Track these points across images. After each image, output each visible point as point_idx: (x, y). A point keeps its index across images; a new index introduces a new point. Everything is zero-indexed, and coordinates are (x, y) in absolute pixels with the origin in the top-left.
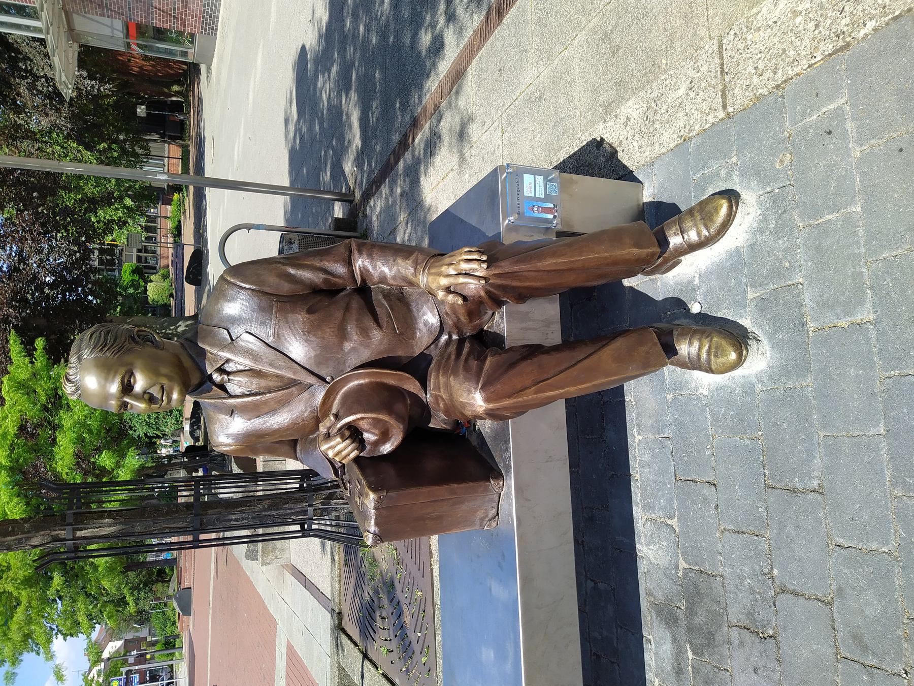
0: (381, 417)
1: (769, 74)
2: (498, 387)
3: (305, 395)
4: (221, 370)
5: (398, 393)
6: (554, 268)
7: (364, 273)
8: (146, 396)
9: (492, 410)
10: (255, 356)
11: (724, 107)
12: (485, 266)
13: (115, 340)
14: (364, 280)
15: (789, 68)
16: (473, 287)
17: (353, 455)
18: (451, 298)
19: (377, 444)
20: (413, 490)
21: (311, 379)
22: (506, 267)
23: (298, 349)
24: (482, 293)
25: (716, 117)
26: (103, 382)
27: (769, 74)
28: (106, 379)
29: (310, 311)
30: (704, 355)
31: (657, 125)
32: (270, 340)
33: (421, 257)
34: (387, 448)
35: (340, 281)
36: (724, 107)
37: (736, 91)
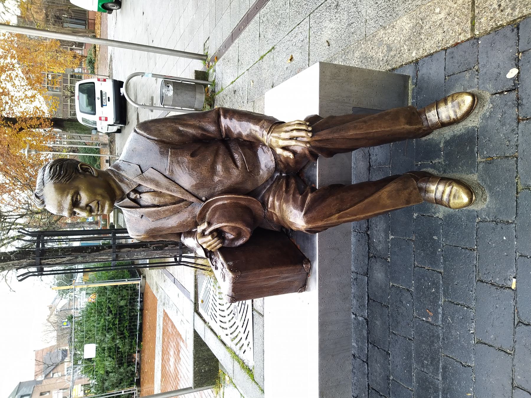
0: (237, 225)
1: (509, 11)
2: (314, 214)
3: (190, 208)
4: (135, 191)
5: (247, 209)
6: (355, 137)
7: (228, 130)
8: (88, 208)
9: (310, 228)
10: (157, 184)
11: (473, 30)
12: (310, 135)
13: (66, 172)
14: (227, 135)
15: (524, 9)
16: (299, 147)
17: (218, 247)
18: (286, 154)
19: (233, 240)
20: (257, 271)
21: (192, 199)
22: (324, 135)
23: (186, 180)
24: (307, 152)
25: (465, 36)
26: (60, 199)
27: (509, 11)
28: (62, 196)
29: (192, 155)
30: (445, 197)
31: (422, 37)
32: (167, 173)
33: (266, 123)
34: (241, 242)
35: (212, 135)
36: (473, 30)
37: (482, 20)
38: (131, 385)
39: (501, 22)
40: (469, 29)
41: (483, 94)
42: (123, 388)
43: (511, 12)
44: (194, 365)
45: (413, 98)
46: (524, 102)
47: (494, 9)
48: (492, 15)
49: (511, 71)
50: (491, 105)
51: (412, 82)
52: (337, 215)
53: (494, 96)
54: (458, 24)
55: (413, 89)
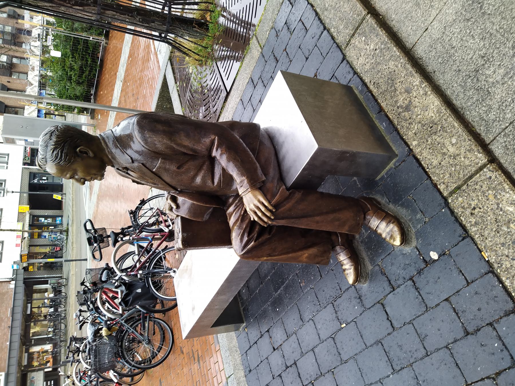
27: (473, 220)
38: (100, 34)
39: (463, 220)
40: (450, 189)
41: (413, 240)
42: (91, 34)
43: (473, 223)
44: (158, 100)
45: (386, 174)
46: (422, 276)
47: (470, 205)
48: (466, 206)
49: (435, 253)
50: (410, 252)
51: (395, 163)
52: (265, 258)
53: (416, 250)
54: (450, 174)
55: (391, 168)
